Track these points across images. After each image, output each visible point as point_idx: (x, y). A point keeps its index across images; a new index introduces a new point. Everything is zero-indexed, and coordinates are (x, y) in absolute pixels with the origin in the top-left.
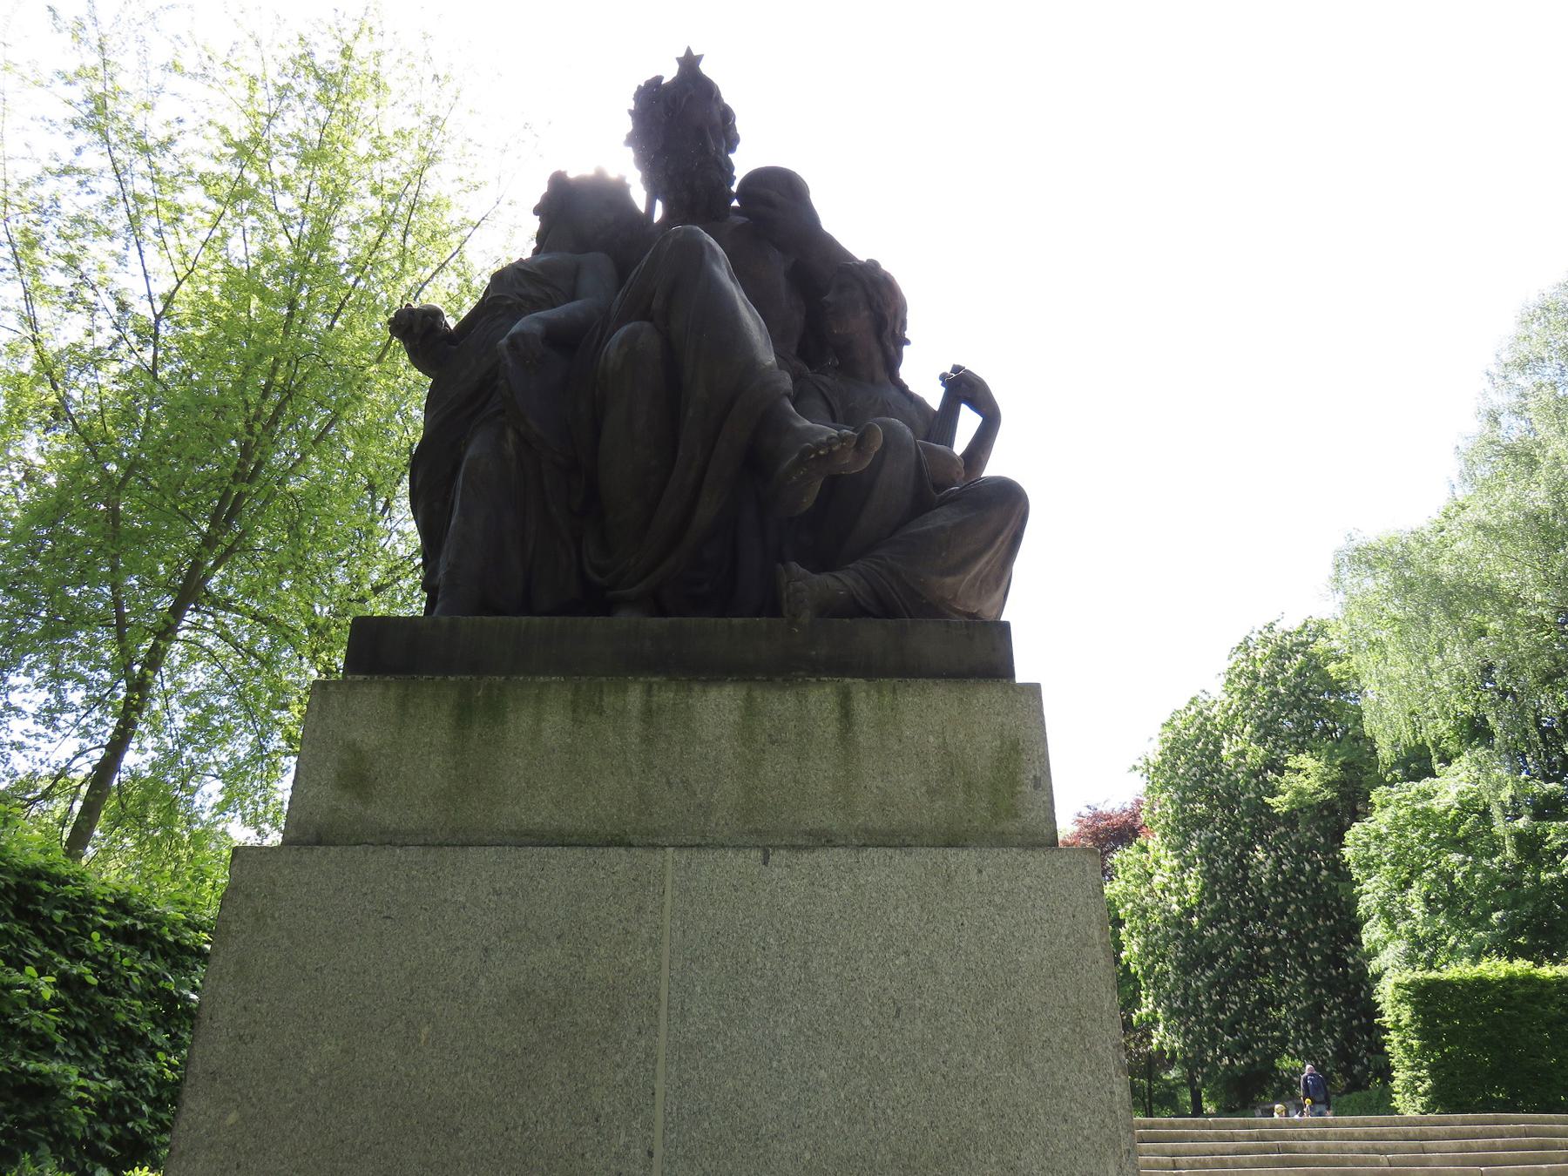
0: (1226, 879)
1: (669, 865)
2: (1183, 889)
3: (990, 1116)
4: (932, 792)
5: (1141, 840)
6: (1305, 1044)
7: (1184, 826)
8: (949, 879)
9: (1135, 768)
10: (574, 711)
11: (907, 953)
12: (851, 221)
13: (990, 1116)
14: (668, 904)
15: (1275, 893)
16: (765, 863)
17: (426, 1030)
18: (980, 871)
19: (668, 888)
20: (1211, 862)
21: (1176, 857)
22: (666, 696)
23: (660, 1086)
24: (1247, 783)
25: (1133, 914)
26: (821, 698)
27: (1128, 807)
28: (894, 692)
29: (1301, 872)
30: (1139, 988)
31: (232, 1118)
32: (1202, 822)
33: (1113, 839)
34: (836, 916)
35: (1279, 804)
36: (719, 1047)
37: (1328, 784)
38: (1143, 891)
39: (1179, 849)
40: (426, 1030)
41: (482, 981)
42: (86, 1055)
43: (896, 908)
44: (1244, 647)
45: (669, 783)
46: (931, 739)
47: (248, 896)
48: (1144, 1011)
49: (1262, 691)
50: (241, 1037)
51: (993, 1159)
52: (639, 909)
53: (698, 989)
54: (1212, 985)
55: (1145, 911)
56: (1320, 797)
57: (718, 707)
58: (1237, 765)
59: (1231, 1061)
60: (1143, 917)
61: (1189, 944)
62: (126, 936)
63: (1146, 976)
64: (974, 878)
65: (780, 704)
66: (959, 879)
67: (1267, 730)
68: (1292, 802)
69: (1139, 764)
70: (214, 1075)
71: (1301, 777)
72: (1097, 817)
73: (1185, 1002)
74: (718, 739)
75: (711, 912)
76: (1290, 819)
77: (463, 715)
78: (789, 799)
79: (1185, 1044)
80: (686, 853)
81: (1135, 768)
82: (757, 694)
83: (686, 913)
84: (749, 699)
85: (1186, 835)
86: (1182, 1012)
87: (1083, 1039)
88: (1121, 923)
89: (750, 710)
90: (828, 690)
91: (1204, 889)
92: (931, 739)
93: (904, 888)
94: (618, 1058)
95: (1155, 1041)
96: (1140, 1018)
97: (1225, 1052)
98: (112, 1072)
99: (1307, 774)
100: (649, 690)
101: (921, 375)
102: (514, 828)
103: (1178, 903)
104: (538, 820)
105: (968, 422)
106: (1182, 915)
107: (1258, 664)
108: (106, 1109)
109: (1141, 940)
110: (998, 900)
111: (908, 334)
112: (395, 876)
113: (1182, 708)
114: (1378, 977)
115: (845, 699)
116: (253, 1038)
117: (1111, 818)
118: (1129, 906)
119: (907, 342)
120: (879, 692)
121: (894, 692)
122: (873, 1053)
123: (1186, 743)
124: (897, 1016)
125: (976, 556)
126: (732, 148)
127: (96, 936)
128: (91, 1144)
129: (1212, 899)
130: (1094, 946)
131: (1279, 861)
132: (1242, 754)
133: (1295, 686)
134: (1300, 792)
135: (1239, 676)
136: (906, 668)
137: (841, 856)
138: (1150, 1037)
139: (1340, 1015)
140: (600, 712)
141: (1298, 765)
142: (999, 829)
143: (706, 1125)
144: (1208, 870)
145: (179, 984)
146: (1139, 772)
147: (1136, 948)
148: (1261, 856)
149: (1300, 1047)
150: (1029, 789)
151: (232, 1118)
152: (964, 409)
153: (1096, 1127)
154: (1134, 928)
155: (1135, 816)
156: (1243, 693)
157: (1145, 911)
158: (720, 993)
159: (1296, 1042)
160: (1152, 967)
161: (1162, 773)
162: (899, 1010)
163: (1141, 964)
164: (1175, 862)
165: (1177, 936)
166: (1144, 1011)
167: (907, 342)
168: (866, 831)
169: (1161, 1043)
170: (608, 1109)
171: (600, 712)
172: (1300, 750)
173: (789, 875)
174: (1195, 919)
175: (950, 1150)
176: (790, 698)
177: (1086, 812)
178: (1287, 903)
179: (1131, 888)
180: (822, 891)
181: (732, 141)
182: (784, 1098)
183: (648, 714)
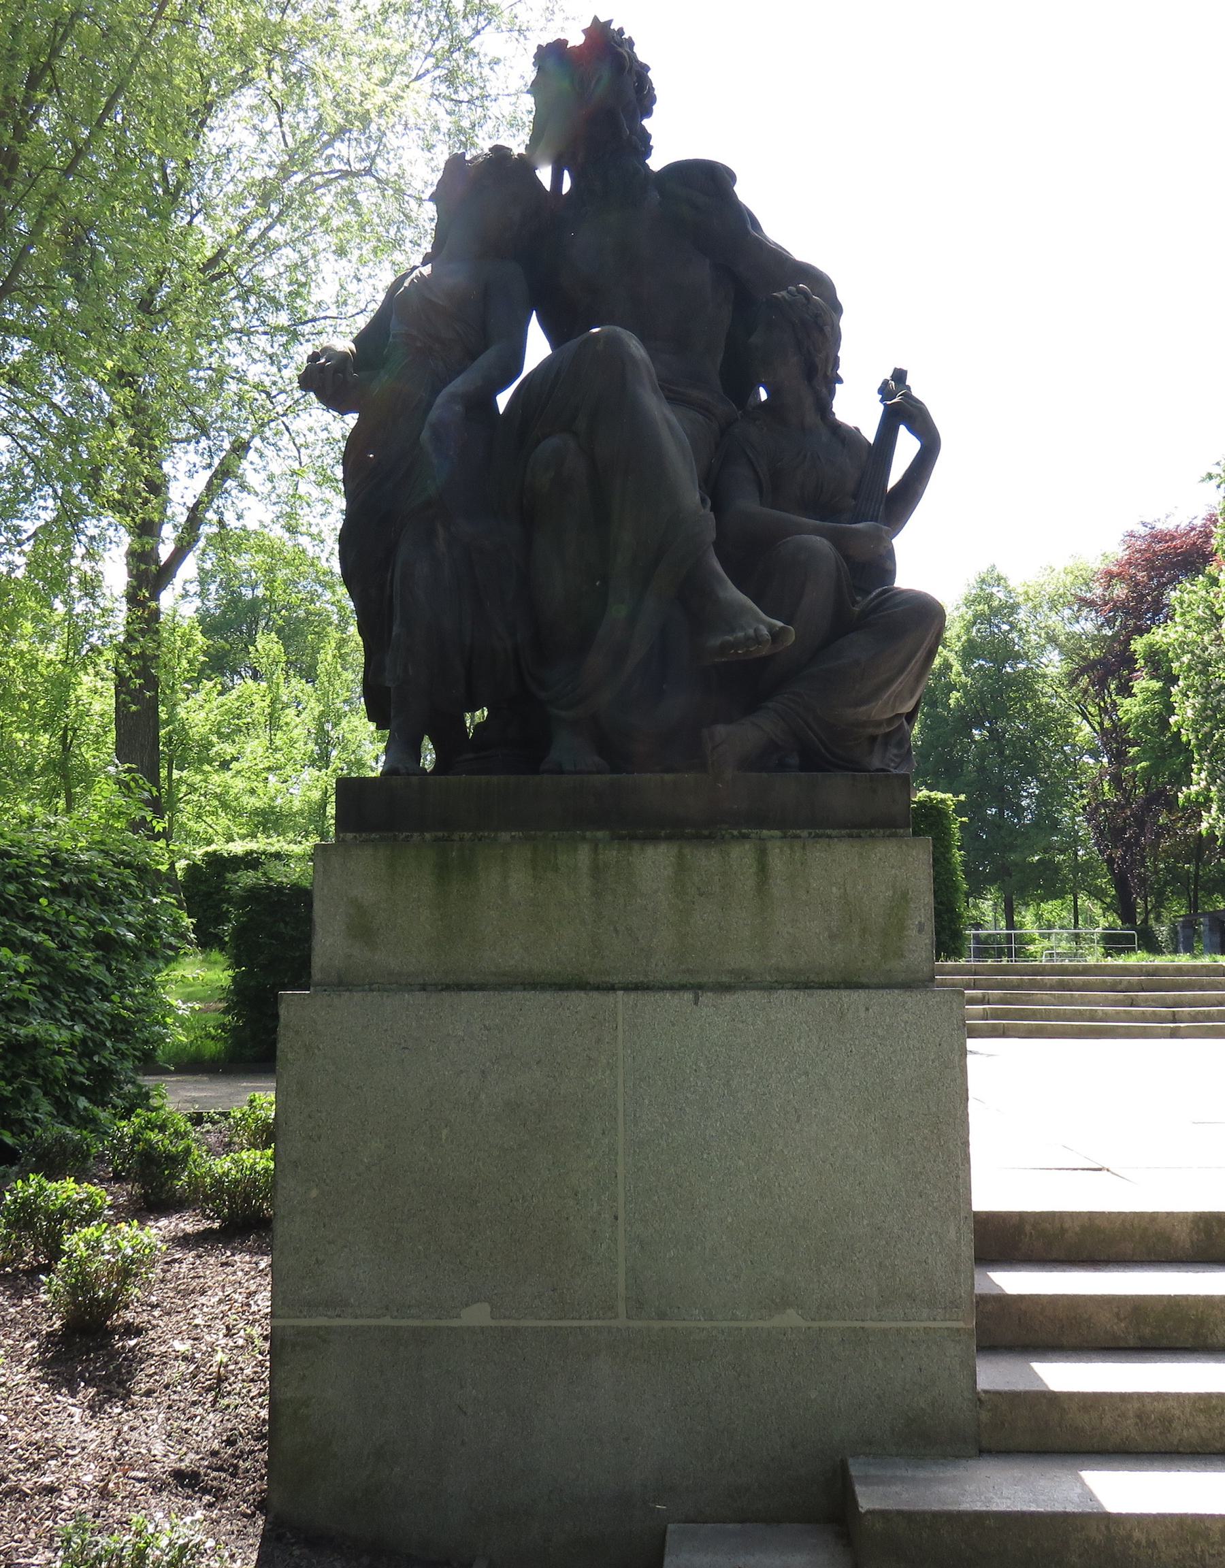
1: (620, 1006)
3: (865, 1193)
4: (832, 937)
5: (1211, 569)
8: (842, 1015)
9: (1210, 476)
10: (534, 869)
11: (807, 1074)
12: (787, 214)
13: (865, 1193)
14: (620, 1036)
16: (696, 1004)
17: (445, 1132)
18: (867, 1009)
19: (620, 1023)
22: (611, 854)
23: (621, 1170)
25: (1190, 668)
26: (741, 855)
27: (1199, 522)
28: (804, 848)
30: (1191, 760)
31: (314, 1193)
33: (1174, 566)
34: (752, 1045)
36: (663, 1143)
38: (1206, 638)
40: (445, 1132)
41: (483, 1096)
42: (52, 1005)
43: (799, 1039)
45: (616, 931)
46: (834, 890)
47: (297, 1032)
50: (310, 1137)
51: (865, 1222)
52: (599, 1041)
53: (647, 1102)
55: (1207, 664)
57: (654, 863)
60: (1204, 672)
62: (65, 890)
63: (1201, 746)
64: (863, 1015)
65: (705, 859)
66: (850, 1016)
70: (296, 1164)
72: (1158, 537)
74: (656, 892)
75: (654, 1043)
77: (443, 871)
78: (714, 943)
80: (633, 995)
81: (1210, 476)
82: (687, 851)
83: (635, 1043)
84: (681, 856)
87: (939, 1138)
88: (1174, 680)
89: (681, 867)
90: (747, 847)
92: (834, 890)
93: (806, 1023)
94: (589, 1151)
96: (1188, 798)
98: (75, 1015)
100: (595, 850)
101: (856, 407)
102: (493, 969)
104: (512, 962)
105: (906, 447)
108: (85, 1049)
110: (880, 1032)
112: (407, 1016)
115: (762, 854)
116: (319, 1138)
117: (1173, 538)
118: (1186, 658)
119: (840, 381)
120: (791, 849)
121: (804, 848)
122: (779, 1148)
124: (798, 1121)
125: (889, 682)
126: (648, 113)
127: (44, 901)
128: (70, 1081)
130: (954, 1068)
136: (814, 822)
137: (757, 997)
138: (1200, 819)
140: (556, 869)
142: (888, 968)
143: (656, 1198)
145: (115, 923)
147: (1190, 713)
150: (914, 933)
151: (314, 1193)
152: (903, 429)
153: (943, 1201)
154: (1190, 687)
155: (1208, 535)
157: (1207, 664)
158: (663, 1104)
162: (799, 1117)
163: (1196, 731)
166: (1194, 788)
167: (840, 381)
168: (778, 969)
169: (1212, 827)
170: (584, 1188)
171: (556, 869)
173: (714, 1013)
175: (834, 1216)
176: (715, 854)
177: (1143, 531)
179: (1191, 635)
180: (740, 1026)
181: (647, 150)
182: (712, 1179)
183: (597, 871)
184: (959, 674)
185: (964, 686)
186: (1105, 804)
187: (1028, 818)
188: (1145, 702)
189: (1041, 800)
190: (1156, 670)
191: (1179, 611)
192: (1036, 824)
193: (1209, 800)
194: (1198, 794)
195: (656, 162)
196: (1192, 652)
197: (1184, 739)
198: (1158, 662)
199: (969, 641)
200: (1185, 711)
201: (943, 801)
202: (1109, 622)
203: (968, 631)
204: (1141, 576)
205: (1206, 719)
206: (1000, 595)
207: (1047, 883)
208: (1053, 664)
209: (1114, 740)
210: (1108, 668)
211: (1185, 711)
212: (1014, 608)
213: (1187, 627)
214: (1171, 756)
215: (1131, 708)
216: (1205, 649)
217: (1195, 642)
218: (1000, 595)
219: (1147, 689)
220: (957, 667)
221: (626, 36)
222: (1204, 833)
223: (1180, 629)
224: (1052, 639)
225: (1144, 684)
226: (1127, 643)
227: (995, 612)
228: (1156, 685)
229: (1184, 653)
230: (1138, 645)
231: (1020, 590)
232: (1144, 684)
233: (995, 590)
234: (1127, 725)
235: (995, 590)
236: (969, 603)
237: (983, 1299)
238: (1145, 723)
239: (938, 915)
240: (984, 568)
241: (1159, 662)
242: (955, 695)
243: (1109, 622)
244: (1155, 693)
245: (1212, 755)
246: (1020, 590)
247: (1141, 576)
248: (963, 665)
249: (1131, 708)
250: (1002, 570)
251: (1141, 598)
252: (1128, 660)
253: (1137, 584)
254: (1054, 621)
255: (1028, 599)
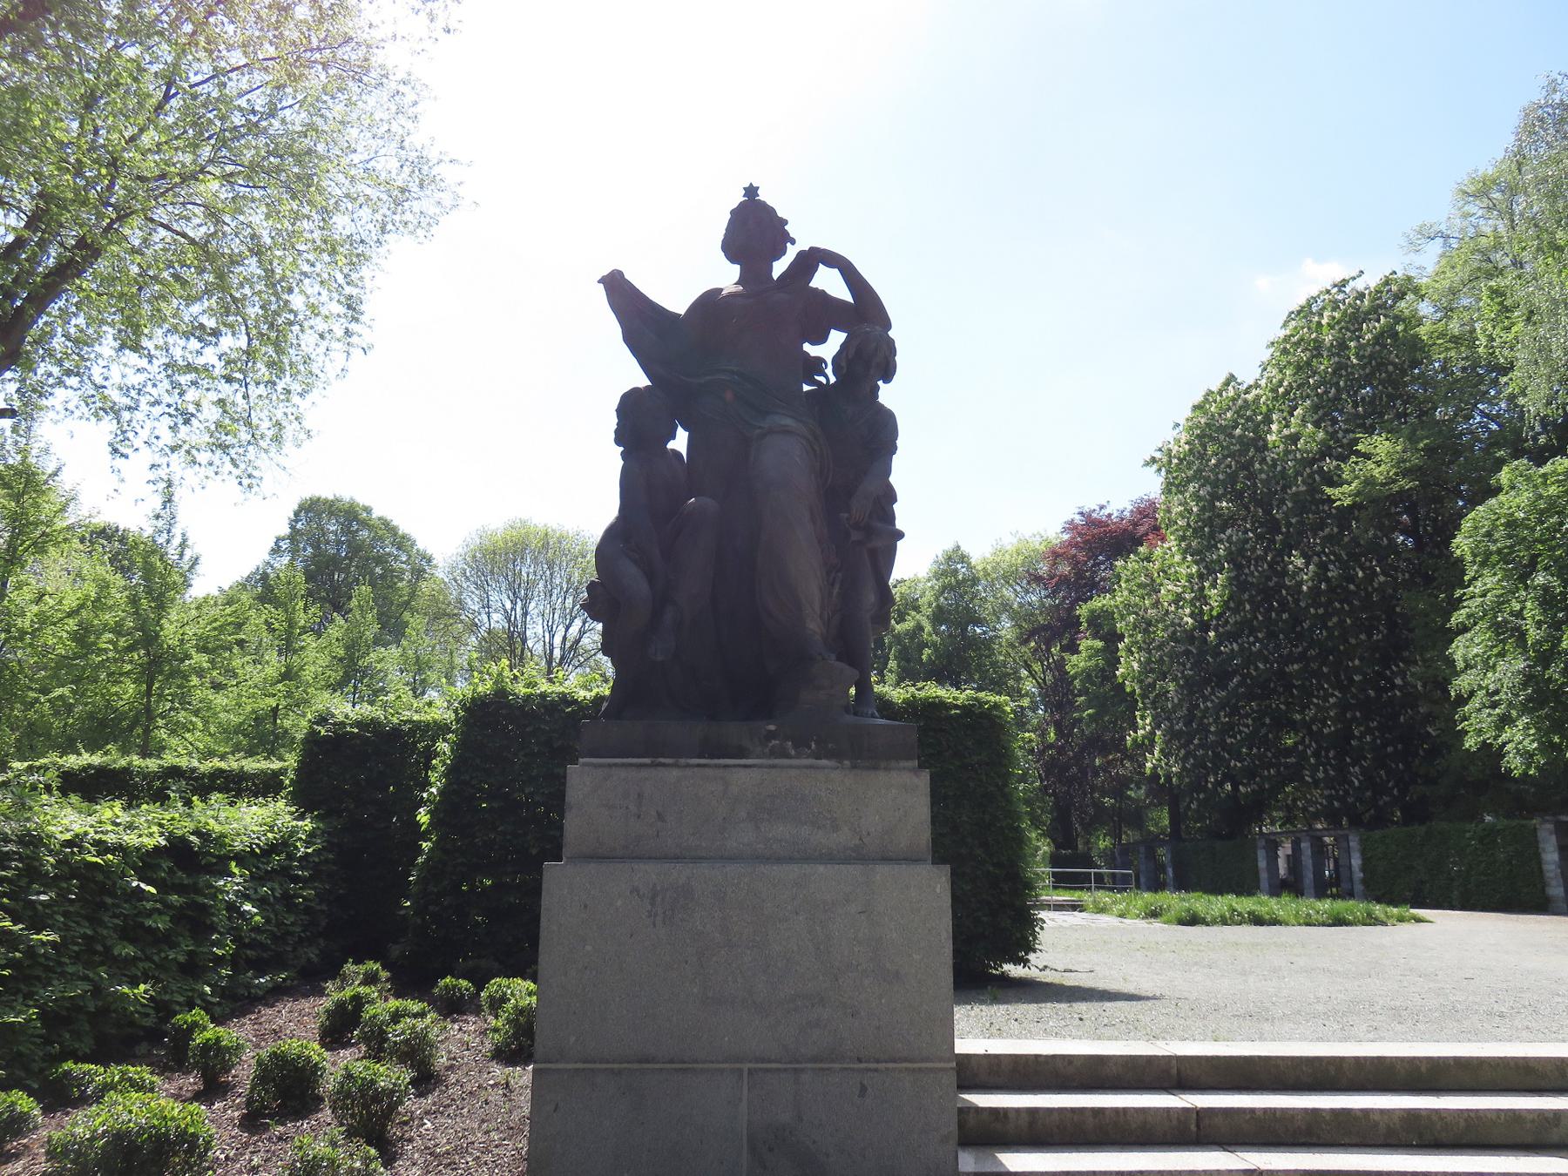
0: (1258, 592)
2: (1202, 597)
6: (1325, 771)
7: (1204, 533)
9: (1154, 460)
15: (1317, 605)
20: (1238, 567)
21: (1196, 562)
24: (1298, 473)
29: (1352, 579)
32: (1229, 521)
35: (1342, 495)
37: (1405, 473)
39: (1199, 555)
44: (1304, 312)
48: (1140, 732)
49: (1324, 365)
54: (1222, 706)
55: (1149, 624)
56: (1395, 488)
58: (1287, 452)
59: (1235, 788)
60: (1146, 631)
61: (1195, 657)
63: (1144, 696)
67: (1323, 412)
68: (1358, 494)
69: (1158, 455)
71: (1370, 465)
73: (1188, 723)
76: (1345, 514)
79: (1183, 768)
85: (1212, 535)
86: (1184, 733)
91: (1231, 598)
95: (1149, 765)
96: (1135, 740)
97: (1228, 777)
99: (1382, 455)
103: (1192, 615)
106: (1194, 629)
107: (1325, 330)
109: (1143, 656)
111: (900, 524)
113: (1215, 389)
114: (1462, 700)
123: (1221, 429)
126: (888, 372)
129: (1236, 611)
131: (1323, 567)
132: (1294, 438)
133: (1371, 357)
134: (1369, 481)
135: (1298, 344)
139: (1374, 740)
141: (1370, 449)
144: (1236, 578)
146: (1155, 467)
148: (1300, 562)
149: (1321, 775)
156: (1299, 368)
159: (1314, 769)
160: (1153, 685)
161: (1180, 469)
163: (1140, 682)
164: (1194, 569)
165: (1187, 653)
166: (1140, 732)
167: (900, 535)
169: (1155, 767)
172: (1370, 431)
174: (1212, 634)
178: (1327, 616)
185: (934, 644)
193: (1152, 743)
194: (1144, 737)
195: (880, 383)
197: (1128, 690)
198: (1103, 626)
200: (1129, 666)
202: (1053, 595)
203: (937, 599)
204: (1081, 556)
205: (1152, 671)
208: (1006, 629)
209: (1058, 694)
210: (1057, 629)
211: (1129, 666)
212: (975, 581)
213: (1131, 592)
214: (1115, 703)
215: (1077, 663)
216: (1146, 610)
219: (1092, 648)
220: (928, 628)
221: (1078, 519)
225: (1088, 643)
226: (1072, 608)
228: (1099, 644)
230: (1083, 611)
231: (979, 568)
232: (1089, 643)
237: (961, 1110)
238: (1089, 676)
240: (949, 546)
242: (927, 651)
245: (1153, 703)
246: (979, 568)
247: (1081, 556)
248: (934, 627)
249: (1077, 663)
250: (965, 549)
252: (1072, 623)
254: (1008, 593)
255: (987, 574)
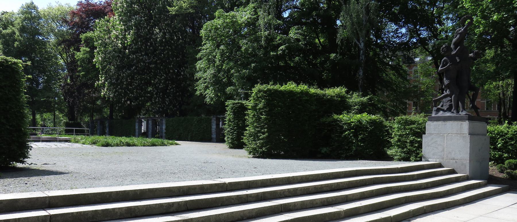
25: (101, 45)
60: (105, 47)
96: (98, 85)
117: (94, 6)
154: (100, 51)
163: (101, 64)
169: (104, 94)
184: (18, 36)
185: (20, 41)
186: (68, 84)
187: (41, 87)
188: (84, 54)
189: (47, 82)
190: (88, 45)
191: (98, 26)
192: (44, 88)
193: (104, 86)
194: (101, 84)
196: (102, 40)
197: (97, 67)
198: (89, 42)
199: (22, 25)
201: (15, 63)
202: (72, 29)
203: (22, 23)
206: (34, 13)
207: (48, 108)
208: (52, 39)
209: (72, 65)
210: (71, 42)
211: (98, 59)
213: (100, 32)
214: (92, 71)
215: (79, 55)
216: (105, 40)
217: (102, 37)
218: (34, 13)
219: (85, 50)
220: (17, 33)
222: (102, 96)
223: (98, 32)
224: (52, 31)
226: (78, 35)
227: (33, 18)
229: (99, 40)
230: (83, 36)
233: (33, 11)
234: (78, 60)
235: (33, 11)
236: (23, 13)
239: (38, 170)
241: (89, 42)
242: (16, 43)
243: (72, 29)
244: (87, 52)
249: (79, 55)
250: (36, 3)
251: (83, 23)
253: (82, 18)
254: (54, 25)
